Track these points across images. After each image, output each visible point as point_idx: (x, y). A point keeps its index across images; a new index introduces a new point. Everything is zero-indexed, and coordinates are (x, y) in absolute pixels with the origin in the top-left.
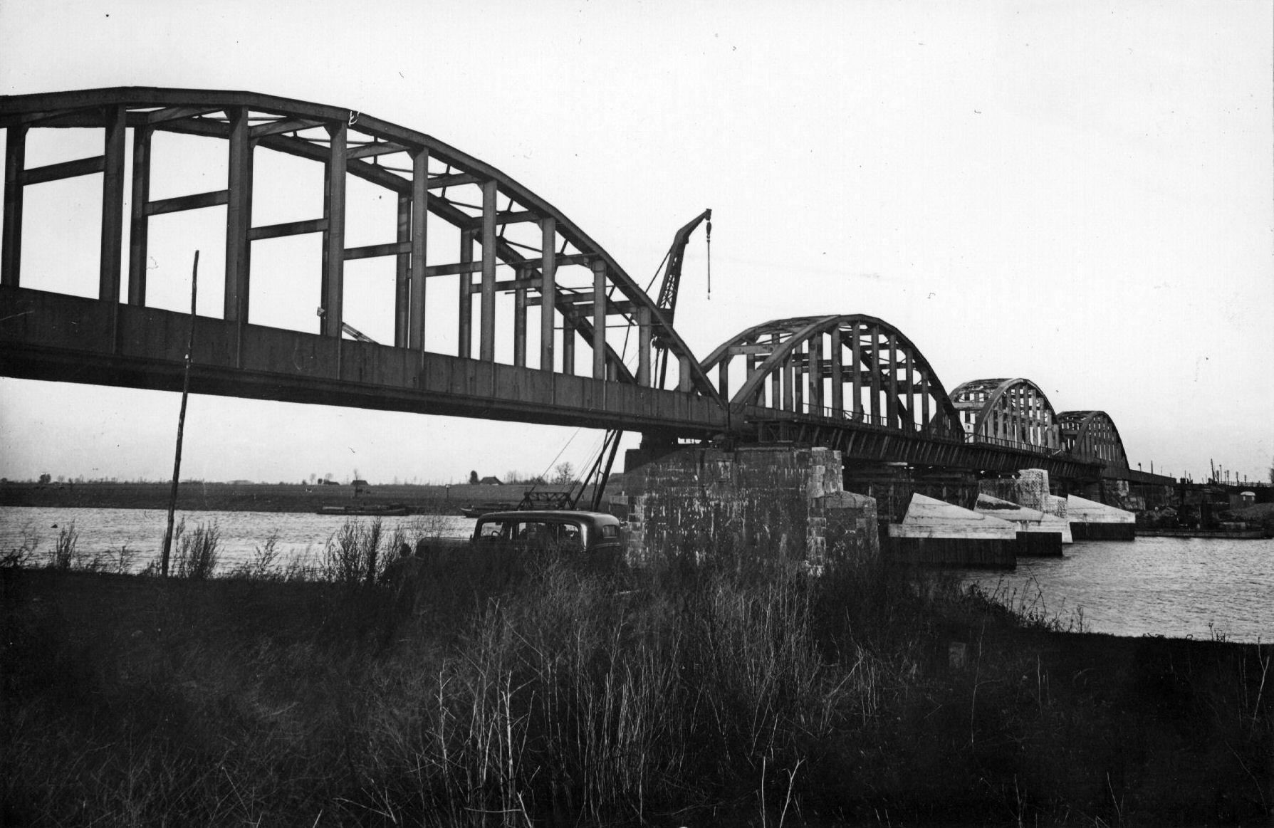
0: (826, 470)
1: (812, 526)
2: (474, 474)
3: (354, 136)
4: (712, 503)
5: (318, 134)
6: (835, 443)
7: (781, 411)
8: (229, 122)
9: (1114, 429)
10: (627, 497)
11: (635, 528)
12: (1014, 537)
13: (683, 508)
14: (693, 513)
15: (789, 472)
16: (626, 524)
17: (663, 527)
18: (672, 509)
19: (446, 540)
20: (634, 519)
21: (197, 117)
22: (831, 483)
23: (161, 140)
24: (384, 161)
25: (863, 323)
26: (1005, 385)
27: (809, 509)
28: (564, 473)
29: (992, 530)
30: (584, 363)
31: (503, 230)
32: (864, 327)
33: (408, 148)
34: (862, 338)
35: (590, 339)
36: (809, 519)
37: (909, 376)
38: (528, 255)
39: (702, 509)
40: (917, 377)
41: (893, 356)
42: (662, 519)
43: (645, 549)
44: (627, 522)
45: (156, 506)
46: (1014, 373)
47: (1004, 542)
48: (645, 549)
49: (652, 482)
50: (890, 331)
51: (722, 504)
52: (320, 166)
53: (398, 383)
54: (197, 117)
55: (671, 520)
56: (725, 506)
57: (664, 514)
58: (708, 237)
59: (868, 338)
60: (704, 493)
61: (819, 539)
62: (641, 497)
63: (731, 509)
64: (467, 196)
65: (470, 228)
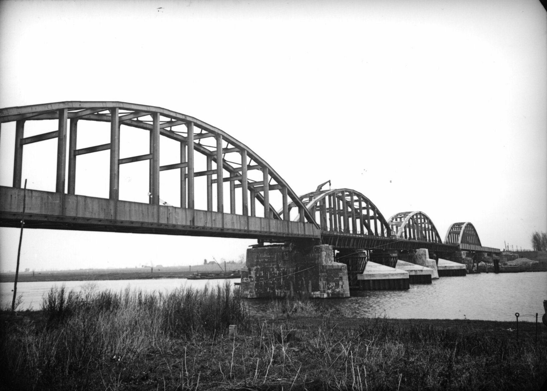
0: (326, 254)
1: (321, 277)
2: (205, 261)
3: (162, 119)
4: (282, 269)
5: (148, 118)
6: (330, 242)
8: (110, 115)
9: (475, 230)
11: (251, 281)
12: (408, 277)
13: (270, 272)
14: (274, 274)
15: (312, 255)
16: (247, 280)
17: (262, 280)
18: (266, 272)
20: (251, 277)
21: (96, 113)
22: (328, 259)
23: (81, 123)
24: (174, 129)
25: (346, 191)
26: (411, 215)
27: (320, 270)
28: (242, 258)
29: (399, 275)
30: (260, 210)
31: (224, 156)
32: (348, 193)
33: (185, 123)
34: (346, 198)
35: (262, 202)
36: (320, 274)
37: (368, 212)
38: (235, 166)
39: (278, 272)
40: (371, 213)
41: (360, 204)
43: (255, 289)
45: (53, 280)
46: (415, 210)
47: (404, 280)
48: (255, 289)
49: (257, 262)
50: (359, 195)
51: (286, 269)
52: (148, 132)
53: (184, 224)
54: (96, 113)
55: (265, 276)
56: (287, 270)
57: (263, 275)
59: (349, 198)
60: (278, 265)
61: (324, 282)
62: (253, 268)
63: (289, 271)
64: (209, 143)
65: (211, 156)
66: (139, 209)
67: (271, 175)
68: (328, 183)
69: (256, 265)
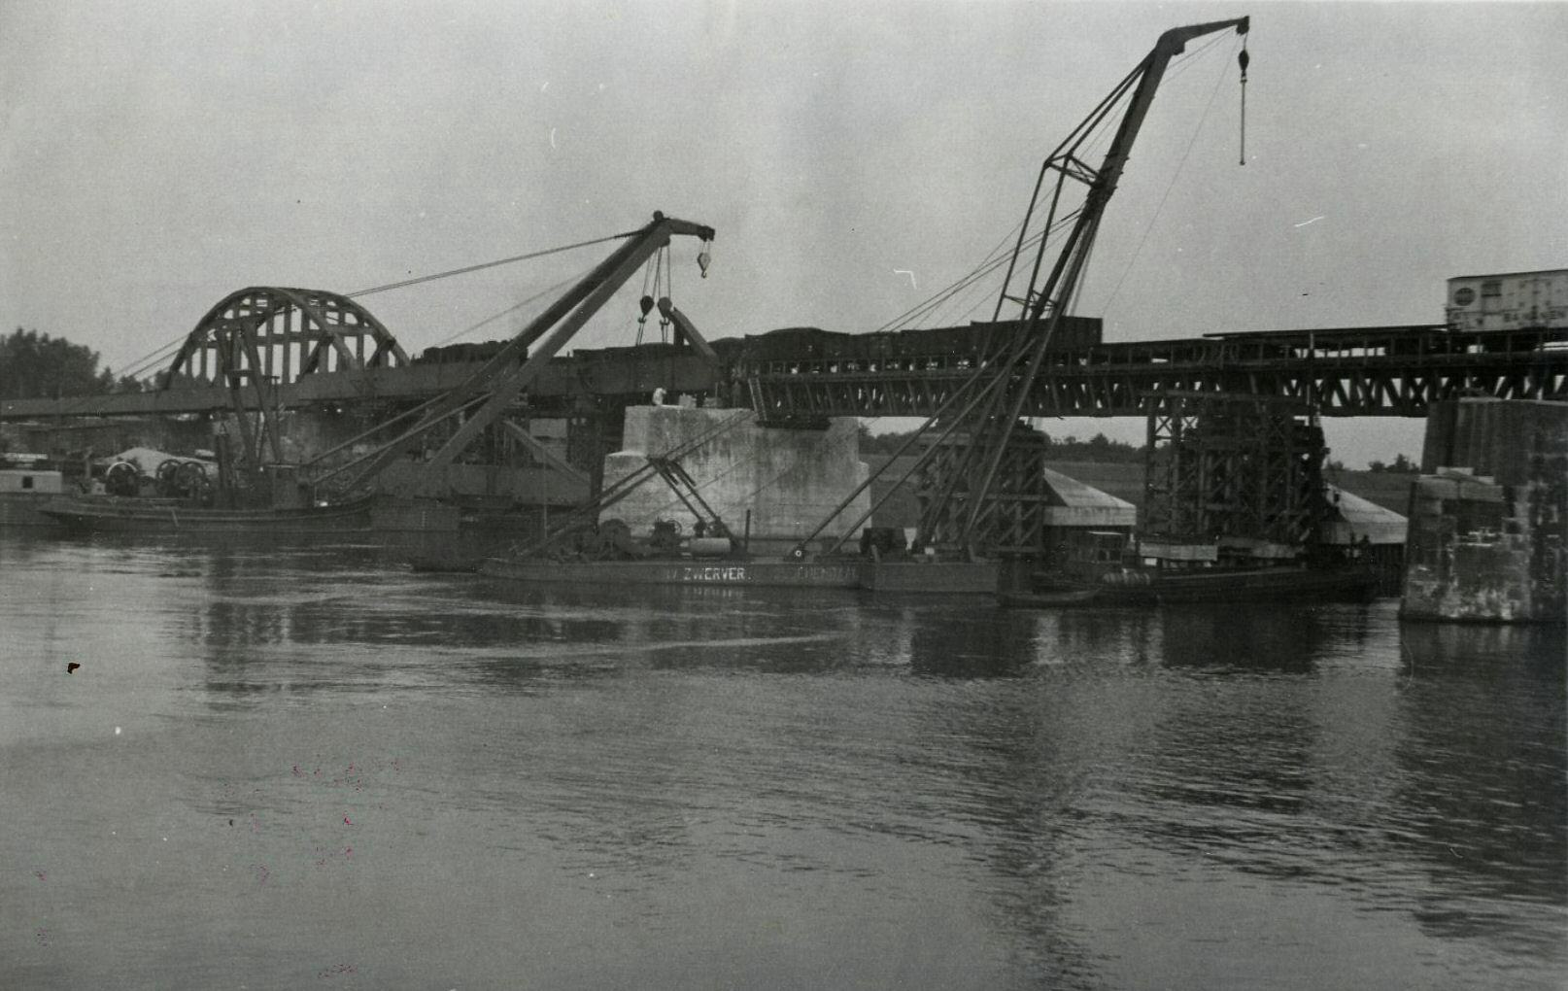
7: (389, 369)
10: (1500, 487)
11: (1516, 545)
16: (1497, 538)
19: (117, 547)
20: (1514, 529)
32: (332, 304)
34: (329, 314)
42: (1555, 529)
43: (1530, 583)
44: (1502, 534)
48: (1530, 583)
58: (1244, 74)
59: (335, 315)
66: (679, 494)
67: (526, 353)
68: (1229, 42)
69: (1534, 477)
